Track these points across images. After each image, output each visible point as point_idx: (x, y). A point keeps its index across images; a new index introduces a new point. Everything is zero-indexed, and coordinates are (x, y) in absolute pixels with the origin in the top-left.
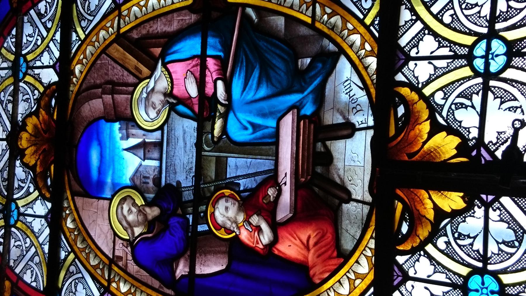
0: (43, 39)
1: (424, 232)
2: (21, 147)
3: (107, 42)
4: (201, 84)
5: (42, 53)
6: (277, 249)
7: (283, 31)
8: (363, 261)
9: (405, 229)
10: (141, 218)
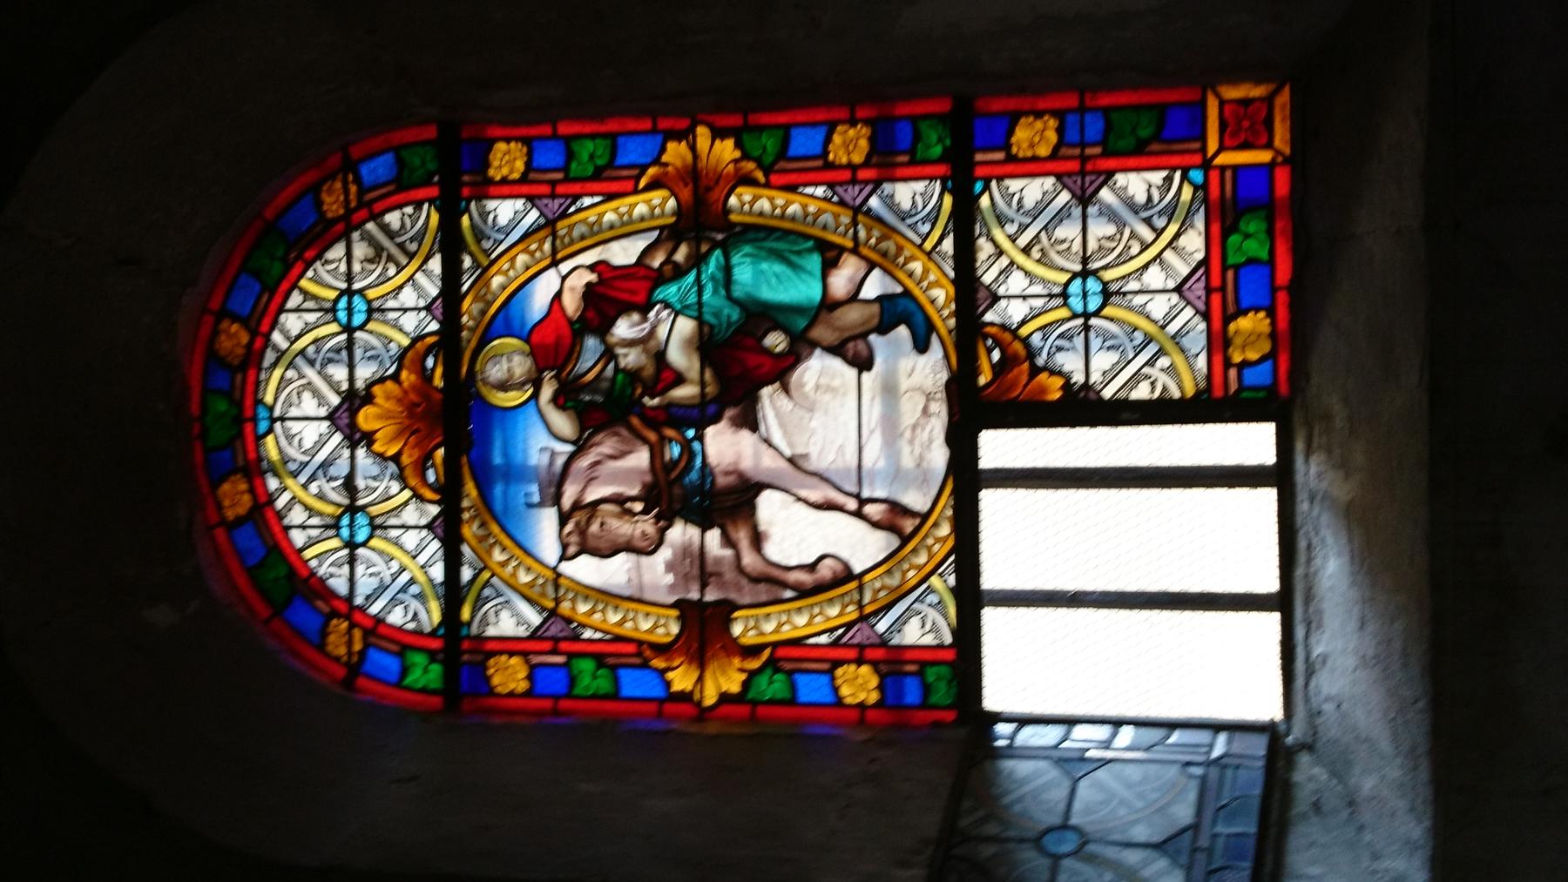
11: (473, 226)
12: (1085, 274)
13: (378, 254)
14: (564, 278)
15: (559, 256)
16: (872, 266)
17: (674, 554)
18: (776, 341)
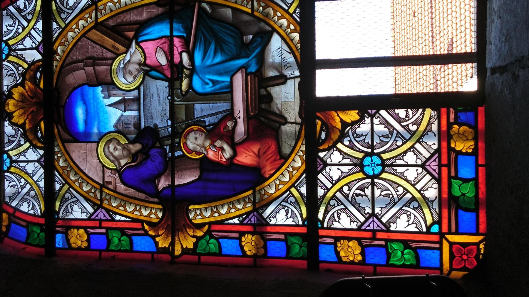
0: (24, 28)
1: (335, 136)
2: (8, 111)
3: (87, 29)
4: (170, 55)
5: (24, 38)
6: (237, 160)
7: (231, 18)
8: (298, 159)
9: (323, 136)
10: (125, 153)
11: (58, 7)
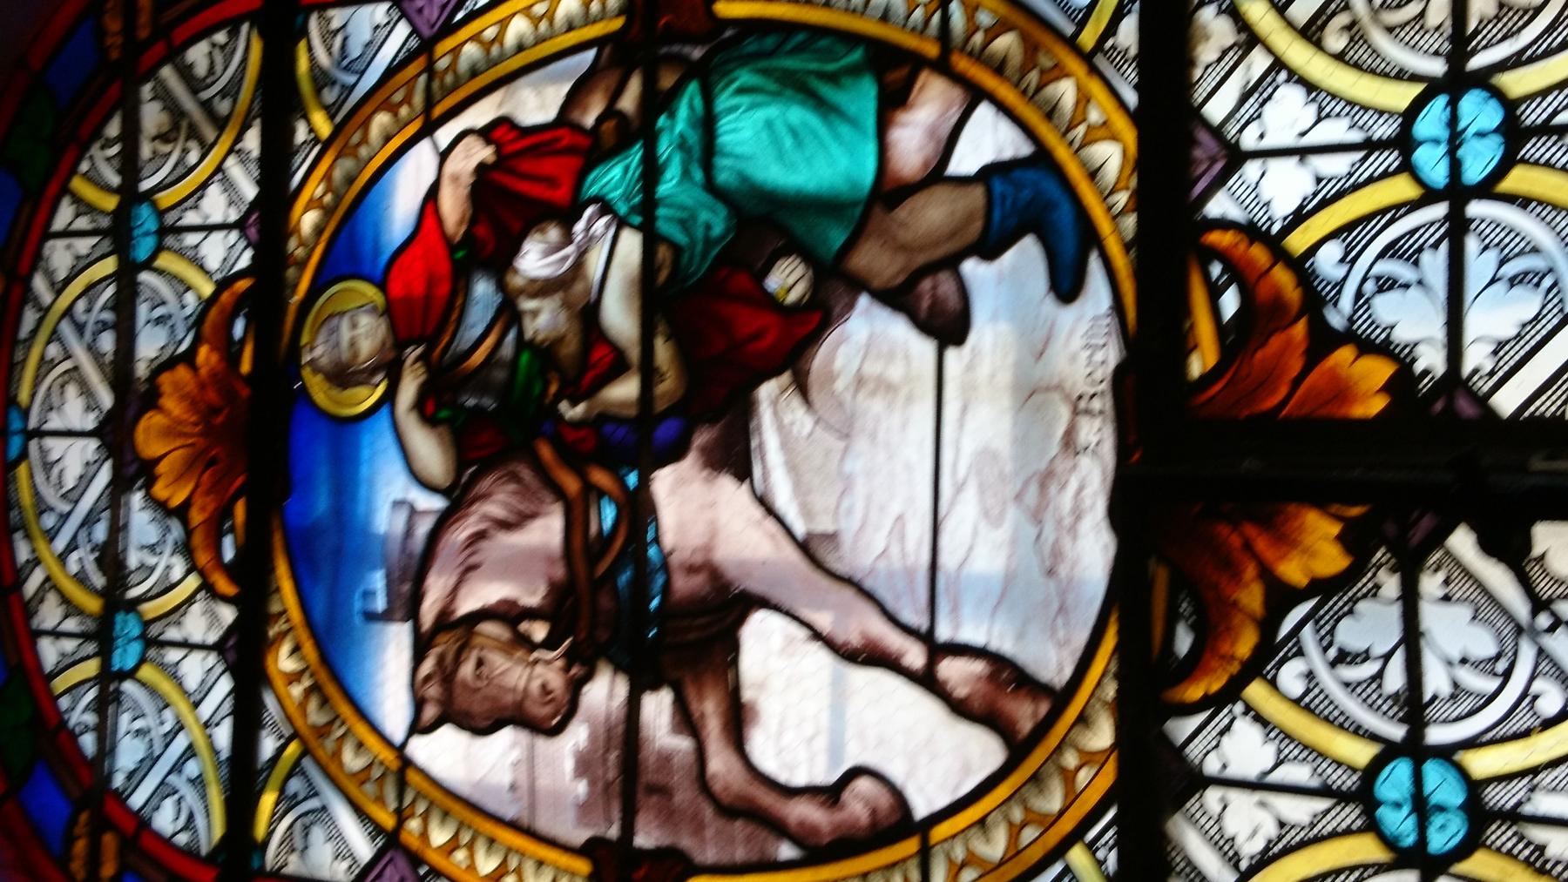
5: (204, 185)
12: (1456, 83)
13: (178, 127)
14: (444, 156)
15: (438, 111)
16: (975, 95)
17: (593, 738)
18: (787, 279)
